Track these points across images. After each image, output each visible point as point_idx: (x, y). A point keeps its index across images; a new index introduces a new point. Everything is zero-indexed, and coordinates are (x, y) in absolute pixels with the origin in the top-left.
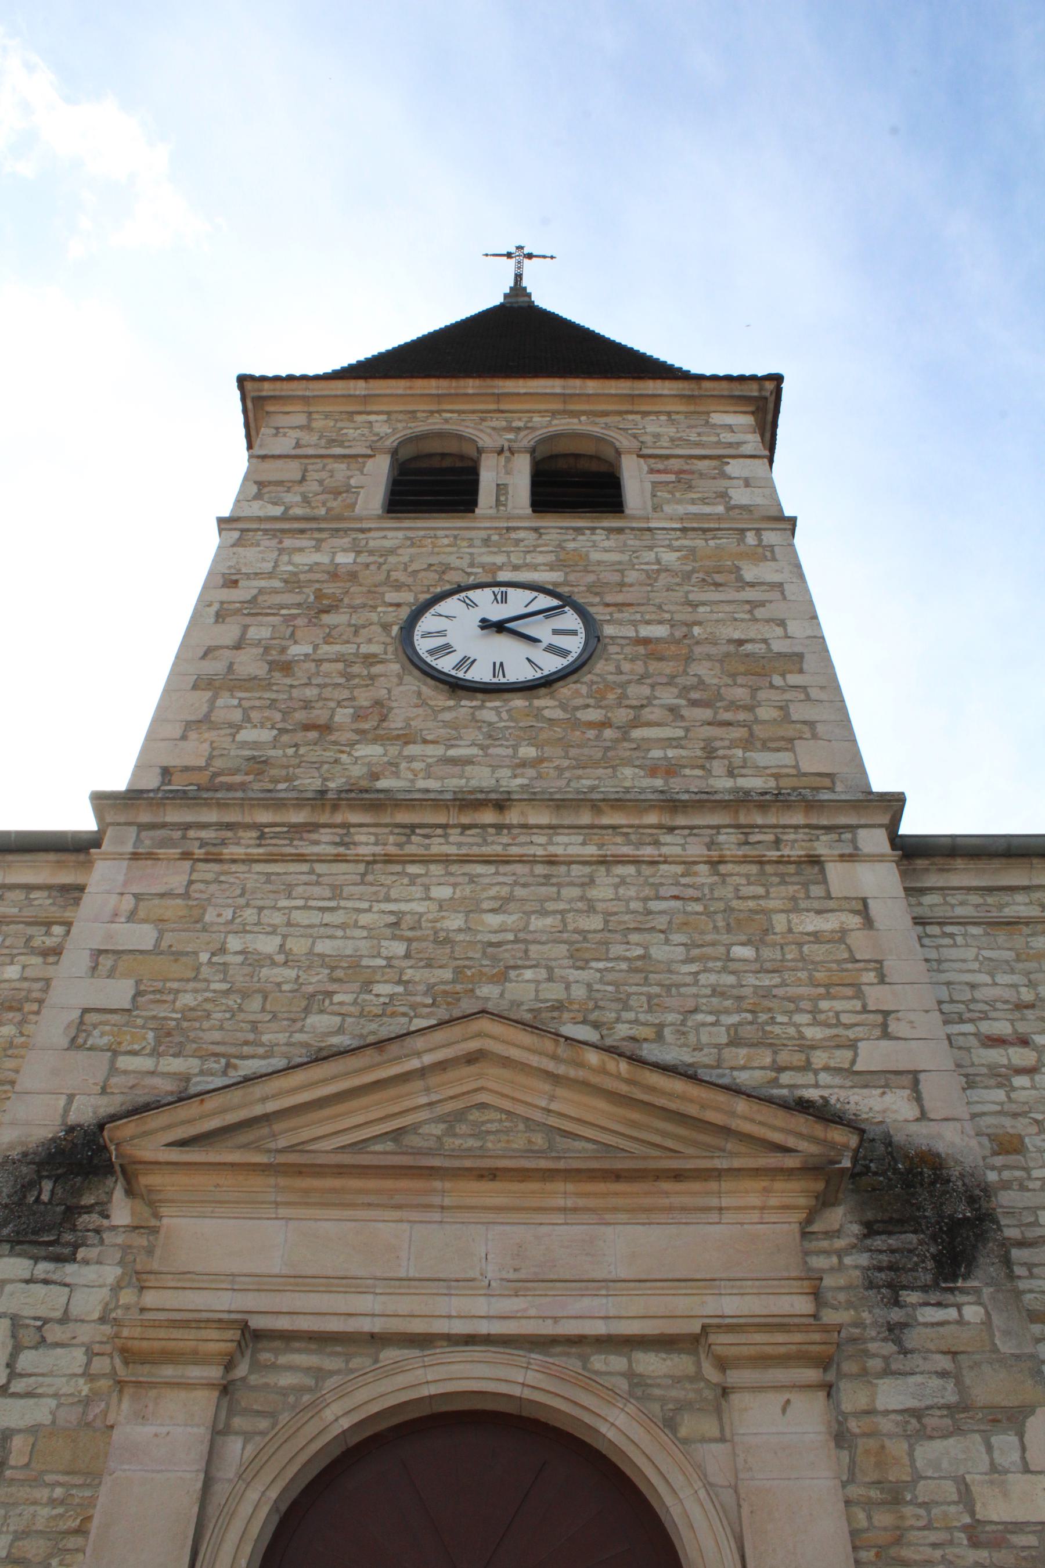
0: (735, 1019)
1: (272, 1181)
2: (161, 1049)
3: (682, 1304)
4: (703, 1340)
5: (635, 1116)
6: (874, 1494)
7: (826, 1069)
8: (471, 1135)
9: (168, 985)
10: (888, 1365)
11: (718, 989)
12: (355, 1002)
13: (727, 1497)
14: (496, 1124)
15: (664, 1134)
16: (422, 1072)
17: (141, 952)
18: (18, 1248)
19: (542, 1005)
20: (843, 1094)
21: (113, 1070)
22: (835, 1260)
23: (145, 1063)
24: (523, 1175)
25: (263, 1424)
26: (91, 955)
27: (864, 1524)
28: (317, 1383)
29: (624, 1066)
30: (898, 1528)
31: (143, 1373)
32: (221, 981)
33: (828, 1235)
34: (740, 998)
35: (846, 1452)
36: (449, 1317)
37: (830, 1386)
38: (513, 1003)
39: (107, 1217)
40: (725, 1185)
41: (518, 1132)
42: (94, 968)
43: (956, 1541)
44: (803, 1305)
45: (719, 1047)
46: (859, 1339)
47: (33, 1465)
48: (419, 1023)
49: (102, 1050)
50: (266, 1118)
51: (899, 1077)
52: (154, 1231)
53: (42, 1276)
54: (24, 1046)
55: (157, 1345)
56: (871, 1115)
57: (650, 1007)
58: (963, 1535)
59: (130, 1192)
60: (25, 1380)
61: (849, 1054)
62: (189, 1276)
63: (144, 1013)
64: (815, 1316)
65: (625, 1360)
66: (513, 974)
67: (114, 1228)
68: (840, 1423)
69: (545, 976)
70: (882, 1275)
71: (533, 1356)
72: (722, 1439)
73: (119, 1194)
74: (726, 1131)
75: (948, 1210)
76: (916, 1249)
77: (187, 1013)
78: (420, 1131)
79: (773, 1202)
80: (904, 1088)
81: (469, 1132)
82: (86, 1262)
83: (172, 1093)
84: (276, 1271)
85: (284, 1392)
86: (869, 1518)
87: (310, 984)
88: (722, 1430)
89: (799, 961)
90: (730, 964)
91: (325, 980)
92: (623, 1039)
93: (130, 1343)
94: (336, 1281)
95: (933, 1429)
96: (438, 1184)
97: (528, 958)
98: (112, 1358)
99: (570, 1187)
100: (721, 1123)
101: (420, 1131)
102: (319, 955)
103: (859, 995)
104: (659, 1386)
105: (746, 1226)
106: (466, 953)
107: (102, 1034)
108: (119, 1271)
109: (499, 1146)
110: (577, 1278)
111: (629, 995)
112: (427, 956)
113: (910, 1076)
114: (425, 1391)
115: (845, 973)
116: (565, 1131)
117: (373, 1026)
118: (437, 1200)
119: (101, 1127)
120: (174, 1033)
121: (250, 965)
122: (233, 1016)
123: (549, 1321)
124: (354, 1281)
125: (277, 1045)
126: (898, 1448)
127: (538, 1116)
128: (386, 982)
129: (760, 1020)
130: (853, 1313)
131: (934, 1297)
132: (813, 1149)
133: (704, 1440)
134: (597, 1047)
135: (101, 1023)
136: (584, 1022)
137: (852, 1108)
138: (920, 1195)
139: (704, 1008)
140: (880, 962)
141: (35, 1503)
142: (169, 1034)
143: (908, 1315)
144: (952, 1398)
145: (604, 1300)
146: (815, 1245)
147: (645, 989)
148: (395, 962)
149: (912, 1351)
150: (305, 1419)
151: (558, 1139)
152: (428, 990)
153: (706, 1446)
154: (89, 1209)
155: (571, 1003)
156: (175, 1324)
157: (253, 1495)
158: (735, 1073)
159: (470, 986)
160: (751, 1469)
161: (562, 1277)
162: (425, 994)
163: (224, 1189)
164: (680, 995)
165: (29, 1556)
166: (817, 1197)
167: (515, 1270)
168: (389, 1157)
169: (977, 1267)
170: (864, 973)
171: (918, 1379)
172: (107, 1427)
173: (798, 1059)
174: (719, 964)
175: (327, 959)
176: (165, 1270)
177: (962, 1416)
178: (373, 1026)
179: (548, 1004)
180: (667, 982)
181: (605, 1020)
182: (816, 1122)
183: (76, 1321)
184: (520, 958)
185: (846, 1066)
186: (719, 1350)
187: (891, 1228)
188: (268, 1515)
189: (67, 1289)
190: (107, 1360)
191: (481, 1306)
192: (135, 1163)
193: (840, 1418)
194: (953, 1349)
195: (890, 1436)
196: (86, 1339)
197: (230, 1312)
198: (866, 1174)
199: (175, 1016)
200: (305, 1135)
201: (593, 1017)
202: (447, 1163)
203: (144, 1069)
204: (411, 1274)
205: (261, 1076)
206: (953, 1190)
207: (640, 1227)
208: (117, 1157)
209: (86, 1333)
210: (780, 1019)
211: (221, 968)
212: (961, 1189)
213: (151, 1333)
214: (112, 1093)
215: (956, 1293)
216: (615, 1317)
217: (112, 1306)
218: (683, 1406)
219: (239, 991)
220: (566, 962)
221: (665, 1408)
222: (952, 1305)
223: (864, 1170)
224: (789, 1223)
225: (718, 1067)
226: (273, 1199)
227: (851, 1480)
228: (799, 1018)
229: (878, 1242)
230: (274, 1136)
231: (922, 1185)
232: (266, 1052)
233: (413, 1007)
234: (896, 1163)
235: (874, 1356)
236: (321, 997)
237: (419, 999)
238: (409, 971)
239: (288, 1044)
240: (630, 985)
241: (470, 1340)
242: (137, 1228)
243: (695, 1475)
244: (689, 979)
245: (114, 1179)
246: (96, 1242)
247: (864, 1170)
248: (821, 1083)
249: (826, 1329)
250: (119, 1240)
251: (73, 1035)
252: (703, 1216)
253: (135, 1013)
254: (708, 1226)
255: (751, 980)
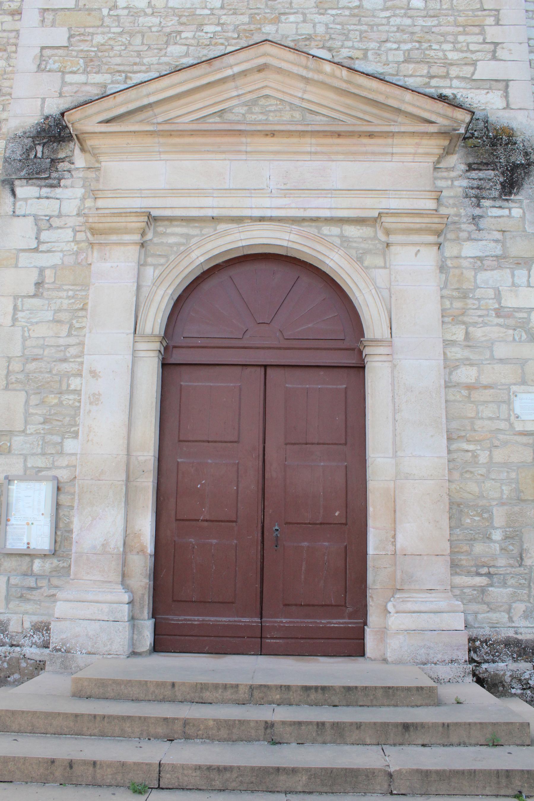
0: (409, 46)
1: (156, 140)
2: (89, 69)
3: (369, 202)
4: (378, 220)
5: (349, 101)
6: (455, 294)
7: (457, 77)
8: (261, 113)
9: (88, 30)
10: (470, 235)
11: (401, 28)
12: (194, 37)
13: (386, 293)
14: (275, 107)
15: (365, 112)
16: (233, 77)
17: (68, 9)
18: (30, 181)
19: (300, 37)
20: (465, 92)
21: (64, 83)
22: (449, 182)
23: (81, 78)
24: (289, 134)
25: (162, 261)
26: (40, 13)
27: (449, 306)
28: (187, 241)
29: (345, 73)
30: (464, 308)
31: (102, 239)
32: (117, 27)
33: (447, 169)
34: (413, 33)
35: (444, 275)
36: (251, 208)
37: (440, 244)
38: (283, 36)
39: (73, 163)
40: (396, 141)
41: (286, 111)
42: (43, 21)
43: (490, 315)
44: (431, 205)
45: (398, 63)
46: (457, 223)
47: (57, 282)
48: (230, 49)
49: (56, 72)
50: (150, 106)
51: (498, 83)
52: (98, 169)
53: (45, 195)
54: (12, 72)
55: (107, 225)
56: (479, 105)
57: (361, 38)
58: (493, 312)
59: (83, 150)
60: (46, 244)
61: (471, 69)
62: (118, 191)
63: (76, 48)
64: (436, 210)
65: (339, 229)
66: (283, 18)
67: (77, 169)
68: (443, 262)
69: (302, 19)
70: (473, 191)
71: (293, 227)
72: (385, 267)
73: (77, 151)
74: (398, 111)
75: (512, 159)
76: (493, 178)
77: (101, 47)
78: (233, 111)
79: (421, 150)
80: (499, 90)
81: (259, 111)
82: (66, 187)
83: (98, 95)
84: (162, 187)
85: (171, 246)
86: (451, 304)
87: (168, 26)
88: (385, 263)
89: (449, 10)
90: (409, 11)
91: (176, 24)
92: (345, 58)
93: (93, 225)
94: (194, 191)
95: (488, 266)
96: (244, 140)
97: (291, 8)
98: (86, 233)
99: (314, 141)
100: (396, 107)
101: (233, 111)
102: (171, 8)
103: (482, 32)
104: (355, 242)
105: (405, 163)
106: (256, 5)
107: (55, 62)
108: (83, 191)
109: (276, 119)
110: (316, 188)
111: (349, 31)
112: (234, 7)
113: (504, 83)
114: (240, 244)
115: (476, 18)
116: (311, 110)
117: (205, 52)
118: (243, 148)
119: (63, 114)
120: (94, 59)
121: (132, 16)
122: (126, 48)
123: (302, 210)
124: (202, 191)
125: (152, 64)
126: (469, 274)
127: (297, 102)
128: (211, 24)
129: (423, 47)
130: (455, 209)
131: (498, 203)
132: (446, 122)
133: (376, 267)
134: (330, 61)
135: (53, 55)
136: (323, 48)
137: (469, 101)
138: (499, 150)
139: (392, 39)
140: (498, 11)
141: (60, 298)
142: (92, 61)
143: (483, 212)
144: (499, 252)
145: (330, 200)
146: (440, 174)
147: (358, 27)
148: (215, 12)
149: (482, 230)
150: (183, 258)
151: (308, 115)
152: (235, 29)
153: (377, 270)
154: (63, 160)
155: (316, 36)
156: (114, 215)
157: (160, 292)
158: (406, 79)
159: (259, 26)
160: (398, 281)
161: (309, 187)
162: (233, 31)
163: (132, 145)
164: (379, 31)
165: (63, 319)
166: (444, 149)
167: (284, 184)
168: (217, 125)
169: (523, 189)
170: (488, 18)
171: (484, 243)
172: (88, 264)
173: (442, 71)
174: (403, 11)
175: (176, 11)
176: (106, 189)
177: (502, 261)
178: (205, 52)
179: (303, 37)
180: (371, 23)
181: (335, 46)
182: (448, 107)
183: (65, 216)
184: (287, 8)
185: (469, 76)
186: (386, 225)
187: (481, 167)
188: (168, 300)
189: (58, 201)
190: (83, 234)
191: (267, 202)
192: (83, 133)
193: (443, 260)
194: (503, 229)
195: (466, 268)
196: (71, 224)
197: (141, 208)
198: (472, 138)
199: (93, 49)
200: (172, 114)
201: (328, 44)
202: (248, 128)
203: (81, 82)
204: (231, 187)
205: (145, 82)
206: (517, 148)
207: (350, 162)
208: (73, 131)
209: (72, 222)
210: (435, 46)
211: (116, 18)
212: (522, 148)
213: (103, 220)
214: (66, 96)
215: (510, 202)
216: (335, 208)
217: (82, 208)
218: (366, 252)
219: (128, 33)
220: (314, 10)
221: (358, 252)
222: (506, 208)
223: (471, 136)
224: (428, 162)
225: (397, 75)
226: (158, 150)
227: (445, 287)
228: (446, 47)
229: (474, 174)
230: (155, 115)
231: (501, 145)
232: (147, 68)
233: (227, 39)
234: (489, 133)
235: (464, 231)
236: (174, 35)
237: (230, 34)
238: (224, 17)
239: (158, 64)
240: (350, 25)
241: (262, 219)
242: (89, 168)
243: (370, 283)
244: (384, 21)
245: (73, 143)
246: (69, 176)
247: (471, 136)
248: (453, 86)
249: (441, 217)
250: (81, 175)
251: (38, 63)
252: (383, 157)
253: (71, 48)
254: (385, 163)
255: (420, 22)
